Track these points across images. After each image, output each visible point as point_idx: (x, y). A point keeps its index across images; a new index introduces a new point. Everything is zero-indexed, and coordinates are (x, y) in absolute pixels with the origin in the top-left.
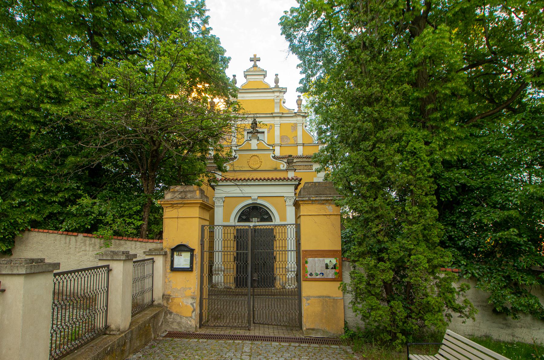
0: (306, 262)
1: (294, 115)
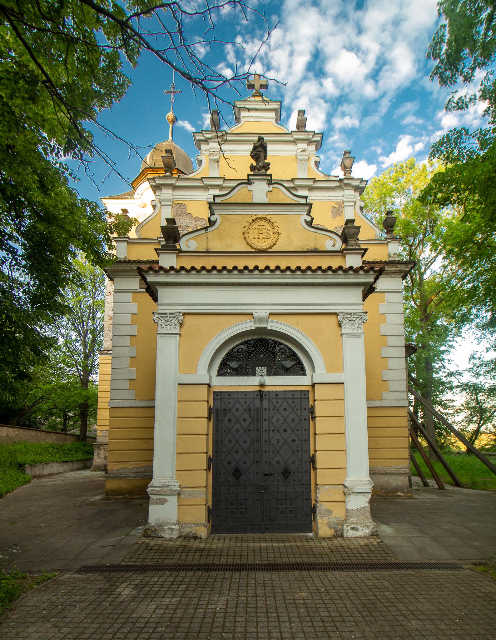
1: (337, 184)
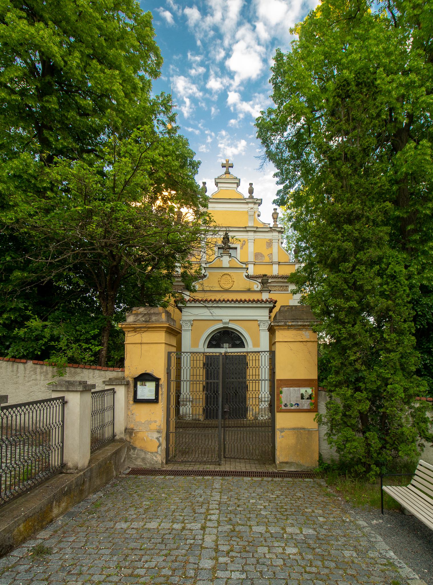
0: (281, 392)
1: (269, 229)
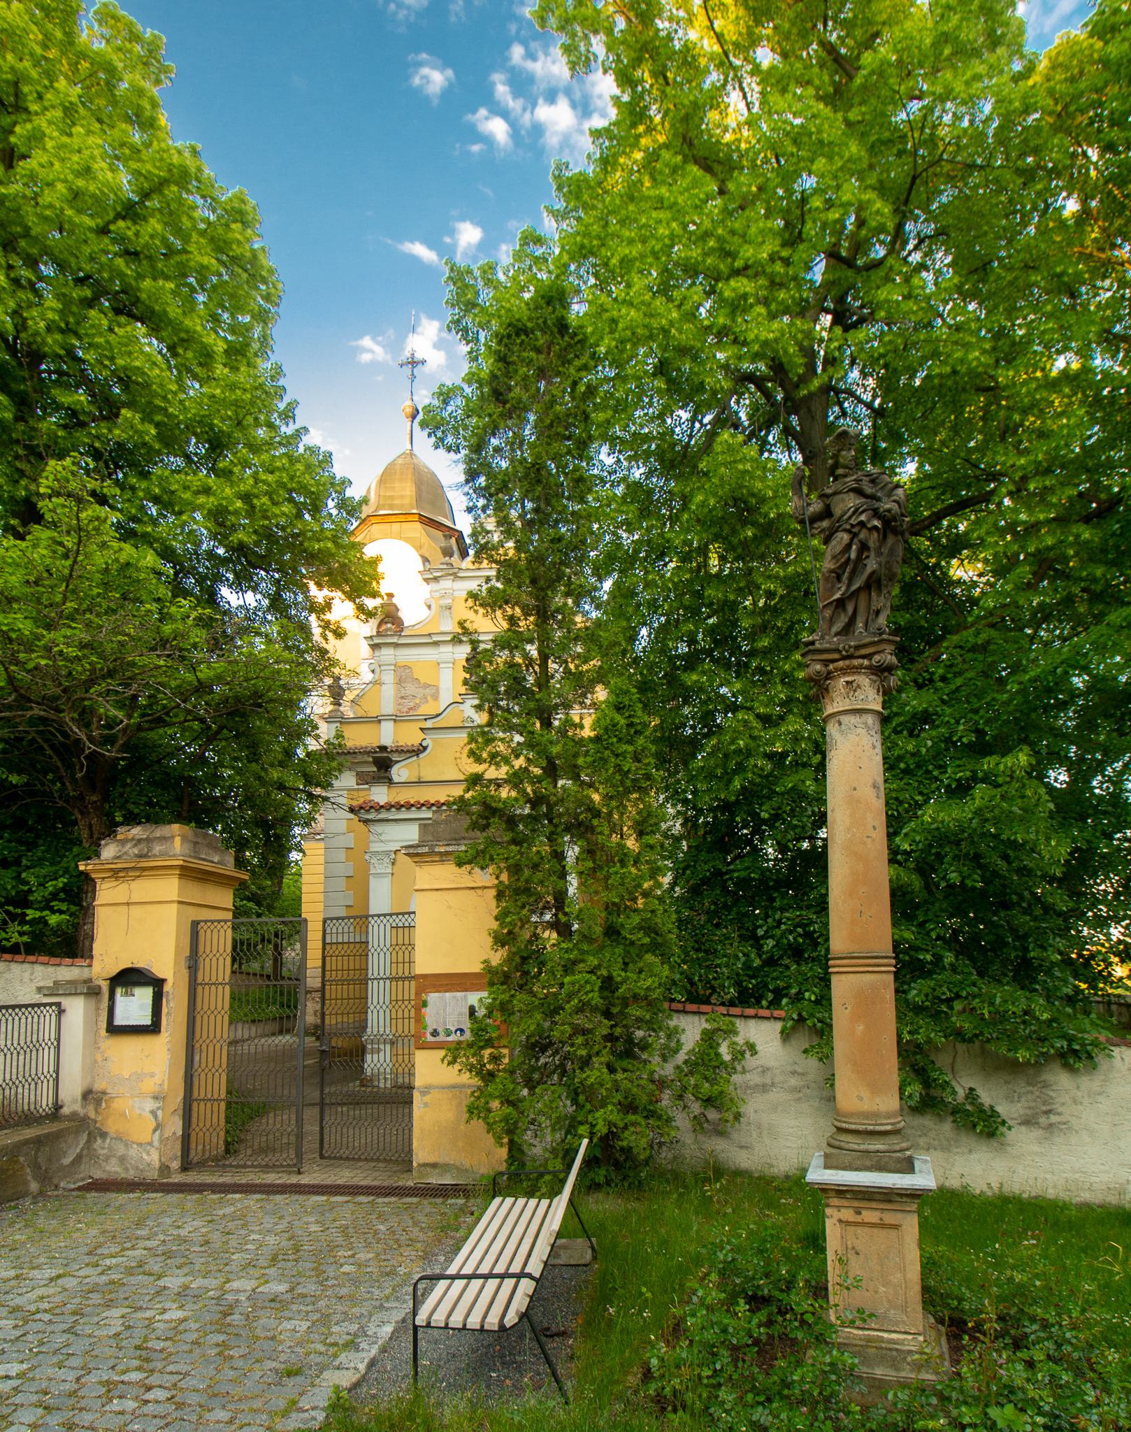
0: (425, 1004)
